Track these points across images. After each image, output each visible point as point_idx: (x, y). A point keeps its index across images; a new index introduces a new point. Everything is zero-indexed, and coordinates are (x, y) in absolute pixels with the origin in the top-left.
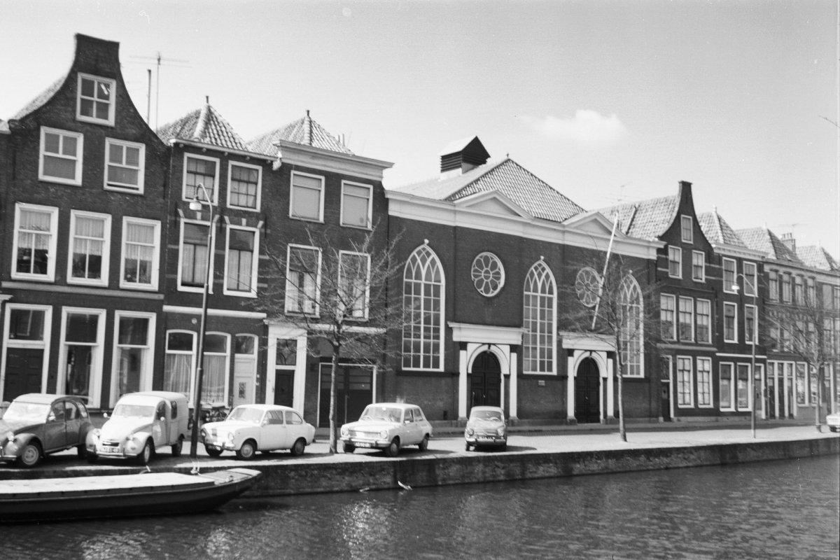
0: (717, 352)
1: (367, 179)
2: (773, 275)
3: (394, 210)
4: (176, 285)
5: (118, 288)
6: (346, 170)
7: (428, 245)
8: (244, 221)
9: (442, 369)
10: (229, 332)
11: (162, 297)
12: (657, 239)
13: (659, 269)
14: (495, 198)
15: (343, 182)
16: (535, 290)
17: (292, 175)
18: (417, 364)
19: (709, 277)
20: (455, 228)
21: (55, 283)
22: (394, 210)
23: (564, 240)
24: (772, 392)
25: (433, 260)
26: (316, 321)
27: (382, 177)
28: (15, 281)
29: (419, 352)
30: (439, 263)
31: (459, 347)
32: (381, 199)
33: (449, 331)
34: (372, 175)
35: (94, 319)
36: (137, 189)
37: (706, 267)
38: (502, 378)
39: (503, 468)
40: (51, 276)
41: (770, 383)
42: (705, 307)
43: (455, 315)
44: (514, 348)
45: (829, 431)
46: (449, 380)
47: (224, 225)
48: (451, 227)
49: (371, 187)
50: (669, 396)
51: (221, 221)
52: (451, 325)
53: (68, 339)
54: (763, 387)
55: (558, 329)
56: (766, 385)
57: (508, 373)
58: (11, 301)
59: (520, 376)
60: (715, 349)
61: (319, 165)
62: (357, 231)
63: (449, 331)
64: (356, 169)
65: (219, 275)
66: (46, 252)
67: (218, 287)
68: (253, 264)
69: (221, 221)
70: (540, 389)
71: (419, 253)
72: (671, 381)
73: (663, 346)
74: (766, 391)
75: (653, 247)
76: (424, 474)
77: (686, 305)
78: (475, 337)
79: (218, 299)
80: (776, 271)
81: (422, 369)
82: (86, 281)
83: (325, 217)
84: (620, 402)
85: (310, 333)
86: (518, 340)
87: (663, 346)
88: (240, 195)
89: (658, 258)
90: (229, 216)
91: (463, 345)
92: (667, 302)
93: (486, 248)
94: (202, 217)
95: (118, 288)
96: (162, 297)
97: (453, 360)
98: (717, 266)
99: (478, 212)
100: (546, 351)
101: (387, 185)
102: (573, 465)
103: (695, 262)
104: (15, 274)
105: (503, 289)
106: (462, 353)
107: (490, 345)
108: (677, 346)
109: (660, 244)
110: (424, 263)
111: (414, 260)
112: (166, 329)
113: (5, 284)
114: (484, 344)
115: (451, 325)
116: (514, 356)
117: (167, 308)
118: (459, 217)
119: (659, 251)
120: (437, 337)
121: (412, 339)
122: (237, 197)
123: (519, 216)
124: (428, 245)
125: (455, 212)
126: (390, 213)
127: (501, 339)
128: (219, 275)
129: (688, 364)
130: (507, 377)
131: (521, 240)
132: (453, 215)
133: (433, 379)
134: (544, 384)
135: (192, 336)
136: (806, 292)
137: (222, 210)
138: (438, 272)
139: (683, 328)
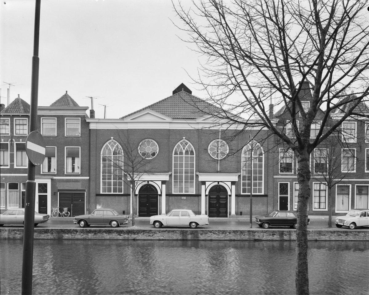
6: (45, 113)
7: (185, 139)
8: (21, 140)
9: (263, 193)
15: (65, 118)
20: (128, 130)
22: (92, 126)
25: (117, 146)
26: (55, 175)
32: (85, 124)
33: (197, 176)
34: (67, 113)
36: (26, 134)
39: (19, 234)
47: (13, 143)
48: (126, 129)
51: (12, 141)
55: (196, 172)
59: (168, 195)
61: (53, 113)
62: (73, 138)
64: (50, 112)
65: (12, 160)
67: (12, 166)
68: (16, 155)
69: (12, 141)
70: (183, 201)
71: (181, 143)
72: (289, 196)
79: (12, 170)
81: (112, 193)
83: (57, 134)
85: (52, 180)
88: (20, 130)
90: (15, 138)
91: (204, 183)
94: (4, 140)
97: (198, 189)
102: (64, 235)
111: (179, 146)
122: (19, 131)
123: (164, 119)
124: (185, 139)
126: (91, 128)
128: (12, 160)
131: (169, 130)
133: (117, 197)
134: (185, 199)
137: (12, 137)
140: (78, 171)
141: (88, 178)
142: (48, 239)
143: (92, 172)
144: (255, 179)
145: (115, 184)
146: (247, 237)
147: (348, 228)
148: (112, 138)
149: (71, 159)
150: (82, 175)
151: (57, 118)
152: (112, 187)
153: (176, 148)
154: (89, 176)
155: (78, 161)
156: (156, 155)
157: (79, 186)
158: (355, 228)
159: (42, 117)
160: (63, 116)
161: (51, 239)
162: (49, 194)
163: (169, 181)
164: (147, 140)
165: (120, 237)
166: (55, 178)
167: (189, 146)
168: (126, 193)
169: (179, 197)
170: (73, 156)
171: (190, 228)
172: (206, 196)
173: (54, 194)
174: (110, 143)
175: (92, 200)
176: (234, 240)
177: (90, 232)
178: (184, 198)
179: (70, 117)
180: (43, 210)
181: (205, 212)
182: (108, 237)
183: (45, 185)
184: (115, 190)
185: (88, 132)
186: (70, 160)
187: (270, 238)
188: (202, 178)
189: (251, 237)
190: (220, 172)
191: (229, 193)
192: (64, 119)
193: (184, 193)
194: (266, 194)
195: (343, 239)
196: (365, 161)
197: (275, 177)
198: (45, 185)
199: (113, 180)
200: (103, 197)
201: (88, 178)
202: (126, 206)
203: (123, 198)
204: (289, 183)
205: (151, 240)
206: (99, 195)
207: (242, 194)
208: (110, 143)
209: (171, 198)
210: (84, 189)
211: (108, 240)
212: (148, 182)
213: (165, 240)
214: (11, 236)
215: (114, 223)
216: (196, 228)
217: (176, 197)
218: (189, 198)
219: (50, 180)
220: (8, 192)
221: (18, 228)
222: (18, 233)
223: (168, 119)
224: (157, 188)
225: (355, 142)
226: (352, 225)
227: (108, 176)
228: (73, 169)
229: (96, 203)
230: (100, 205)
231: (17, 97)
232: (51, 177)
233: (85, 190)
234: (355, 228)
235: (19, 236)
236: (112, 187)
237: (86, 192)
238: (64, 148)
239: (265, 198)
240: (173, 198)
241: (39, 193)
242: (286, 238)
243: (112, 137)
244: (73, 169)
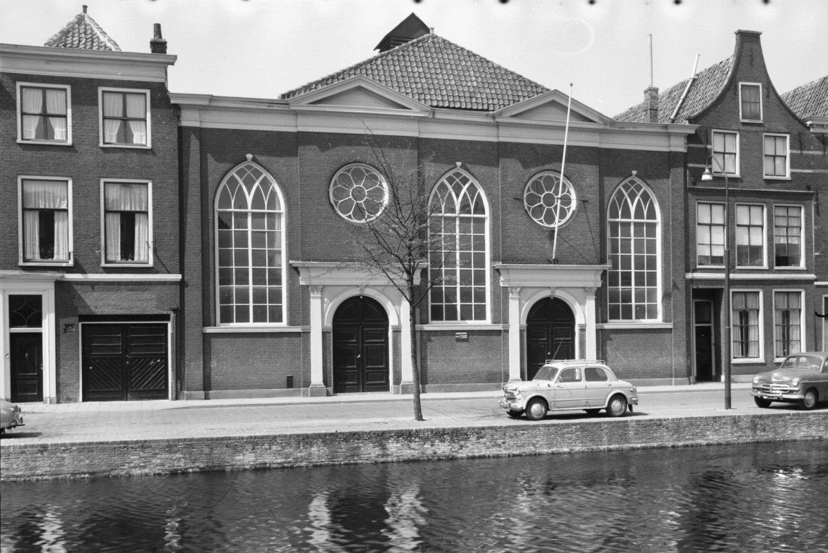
0: (816, 280)
1: (138, 82)
3: (189, 120)
7: (636, 175)
10: (822, 297)
12: (687, 123)
14: (553, 101)
15: (100, 89)
16: (626, 214)
17: (712, 133)
19: (794, 171)
23: (669, 146)
45: (755, 405)
49: (148, 92)
60: (812, 276)
75: (677, 135)
84: (713, 359)
86: (596, 281)
88: (726, 155)
89: (689, 149)
99: (539, 123)
100: (473, 291)
101: (174, 87)
109: (691, 129)
118: (503, 131)
119: (690, 138)
121: (234, 286)
124: (254, 160)
125: (497, 125)
126: (184, 124)
130: (397, 331)
132: (293, 117)
143: (193, 259)
145: (259, 296)
148: (634, 172)
149: (119, 218)
150: (807, 271)
151: (151, 93)
152: (251, 304)
153: (465, 194)
154: (182, 271)
157: (146, 304)
159: (20, 80)
160: (91, 80)
162: (48, 328)
163: (419, 286)
166: (70, 277)
173: (61, 331)
179: (116, 86)
181: (519, 375)
183: (37, 300)
185: (174, 137)
190: (556, 261)
192: (97, 90)
196: (459, 225)
198: (37, 300)
201: (178, 277)
208: (240, 173)
210: (165, 313)
227: (446, 272)
232: (58, 275)
233: (167, 317)
236: (251, 304)
238: (99, 184)
241: (248, 321)
243: (634, 170)
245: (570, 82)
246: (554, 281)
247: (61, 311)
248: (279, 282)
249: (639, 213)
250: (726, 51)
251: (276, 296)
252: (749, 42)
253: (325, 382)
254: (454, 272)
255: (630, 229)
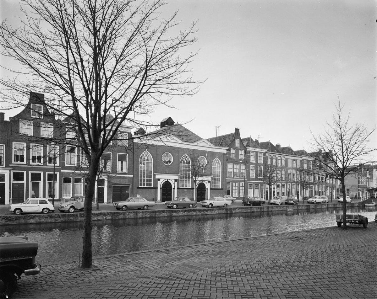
2: (269, 157)
4: (65, 164)
5: (47, 166)
9: (221, 188)
11: (61, 168)
13: (227, 156)
16: (215, 165)
18: (144, 185)
21: (26, 164)
24: (267, 192)
26: (110, 173)
27: (131, 131)
28: (32, 165)
29: (146, 183)
30: (220, 162)
31: (157, 180)
33: (154, 175)
35: (40, 174)
37: (244, 155)
38: (206, 189)
40: (25, 162)
41: (298, 190)
42: (243, 167)
43: (156, 171)
44: (176, 180)
46: (154, 190)
49: (128, 134)
50: (129, 192)
52: (155, 174)
53: (48, 181)
54: (264, 191)
56: (265, 190)
57: (174, 187)
58: (12, 170)
59: (178, 188)
63: (154, 175)
66: (23, 156)
73: (228, 179)
74: (265, 192)
76: (122, 216)
77: (237, 166)
78: (163, 178)
80: (280, 157)
81: (146, 187)
82: (19, 162)
85: (108, 176)
87: (228, 179)
91: (159, 180)
92: (230, 166)
93: (202, 155)
95: (47, 166)
96: (61, 168)
97: (156, 183)
98: (248, 154)
102: (173, 214)
103: (240, 153)
104: (13, 162)
105: (172, 163)
106: (159, 182)
107: (168, 179)
108: (233, 179)
110: (216, 162)
112: (62, 177)
113: (10, 165)
114: (166, 179)
115: (155, 174)
116: (176, 183)
117: (62, 171)
120: (151, 177)
124: (147, 150)
126: (134, 142)
127: (172, 178)
129: (237, 184)
131: (179, 148)
135: (71, 178)
136: (281, 162)
138: (220, 164)
139: (235, 174)
140: (125, 170)
141: (132, 176)
142: (165, 217)
143: (135, 172)
144: (217, 180)
145: (147, 180)
146: (250, 210)
147: (208, 206)
150: (128, 174)
155: (125, 164)
156: (171, 163)
157: (126, 182)
158: (21, 214)
161: (166, 217)
164: (166, 153)
165: (200, 214)
167: (188, 159)
168: (155, 187)
169: (183, 190)
170: (122, 159)
171: (15, 214)
172: (160, 188)
173: (109, 187)
174: (144, 153)
175: (135, 192)
176: (245, 212)
177: (186, 211)
178: (186, 190)
180: (101, 199)
182: (195, 214)
184: (186, 186)
186: (120, 162)
187: (247, 211)
188: (157, 177)
189: (251, 210)
191: (173, 187)
193: (185, 187)
194: (222, 188)
195: (279, 210)
197: (226, 179)
199: (147, 178)
200: (141, 189)
201: (132, 176)
202: (155, 195)
203: (153, 190)
204: (72, 178)
205: (214, 214)
206: (138, 188)
207: (140, 187)
209: (179, 190)
211: (194, 215)
212: (168, 180)
213: (219, 214)
214: (144, 216)
215: (191, 205)
216: (212, 207)
217: (182, 190)
218: (188, 190)
219: (106, 176)
220: (231, 188)
221: (39, 214)
222: (148, 213)
223: (180, 141)
224: (172, 185)
225: (273, 164)
226: (210, 205)
228: (122, 169)
229: (137, 193)
230: (139, 195)
231: (249, 137)
233: (130, 185)
234: (21, 214)
235: (148, 215)
237: (131, 186)
239: (222, 190)
240: (180, 190)
242: (262, 210)
244: (122, 169)
245: (373, 79)
246: (37, 165)
247: (109, 182)
248: (151, 178)
249: (218, 166)
250: (233, 131)
251: (151, 181)
252: (237, 130)
253: (160, 200)
254: (145, 175)
255: (64, 172)
